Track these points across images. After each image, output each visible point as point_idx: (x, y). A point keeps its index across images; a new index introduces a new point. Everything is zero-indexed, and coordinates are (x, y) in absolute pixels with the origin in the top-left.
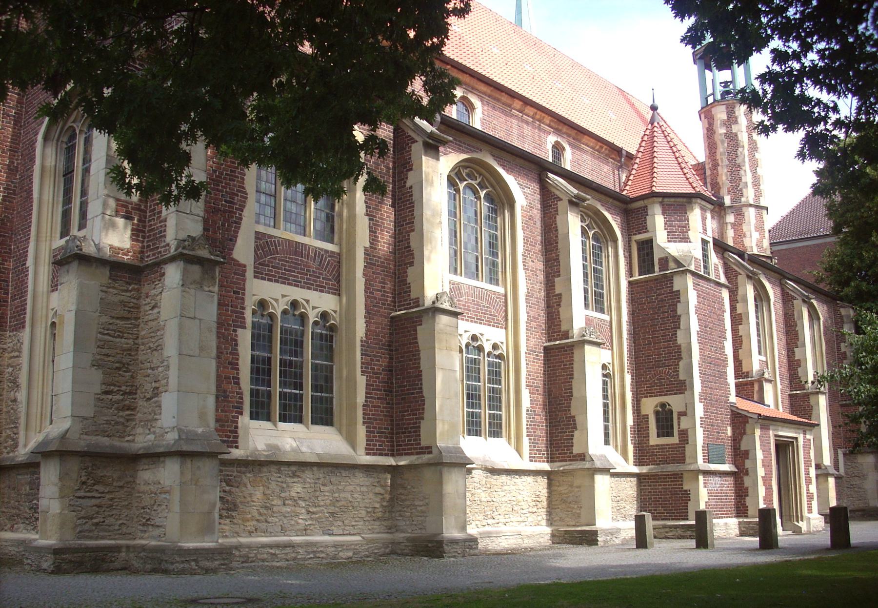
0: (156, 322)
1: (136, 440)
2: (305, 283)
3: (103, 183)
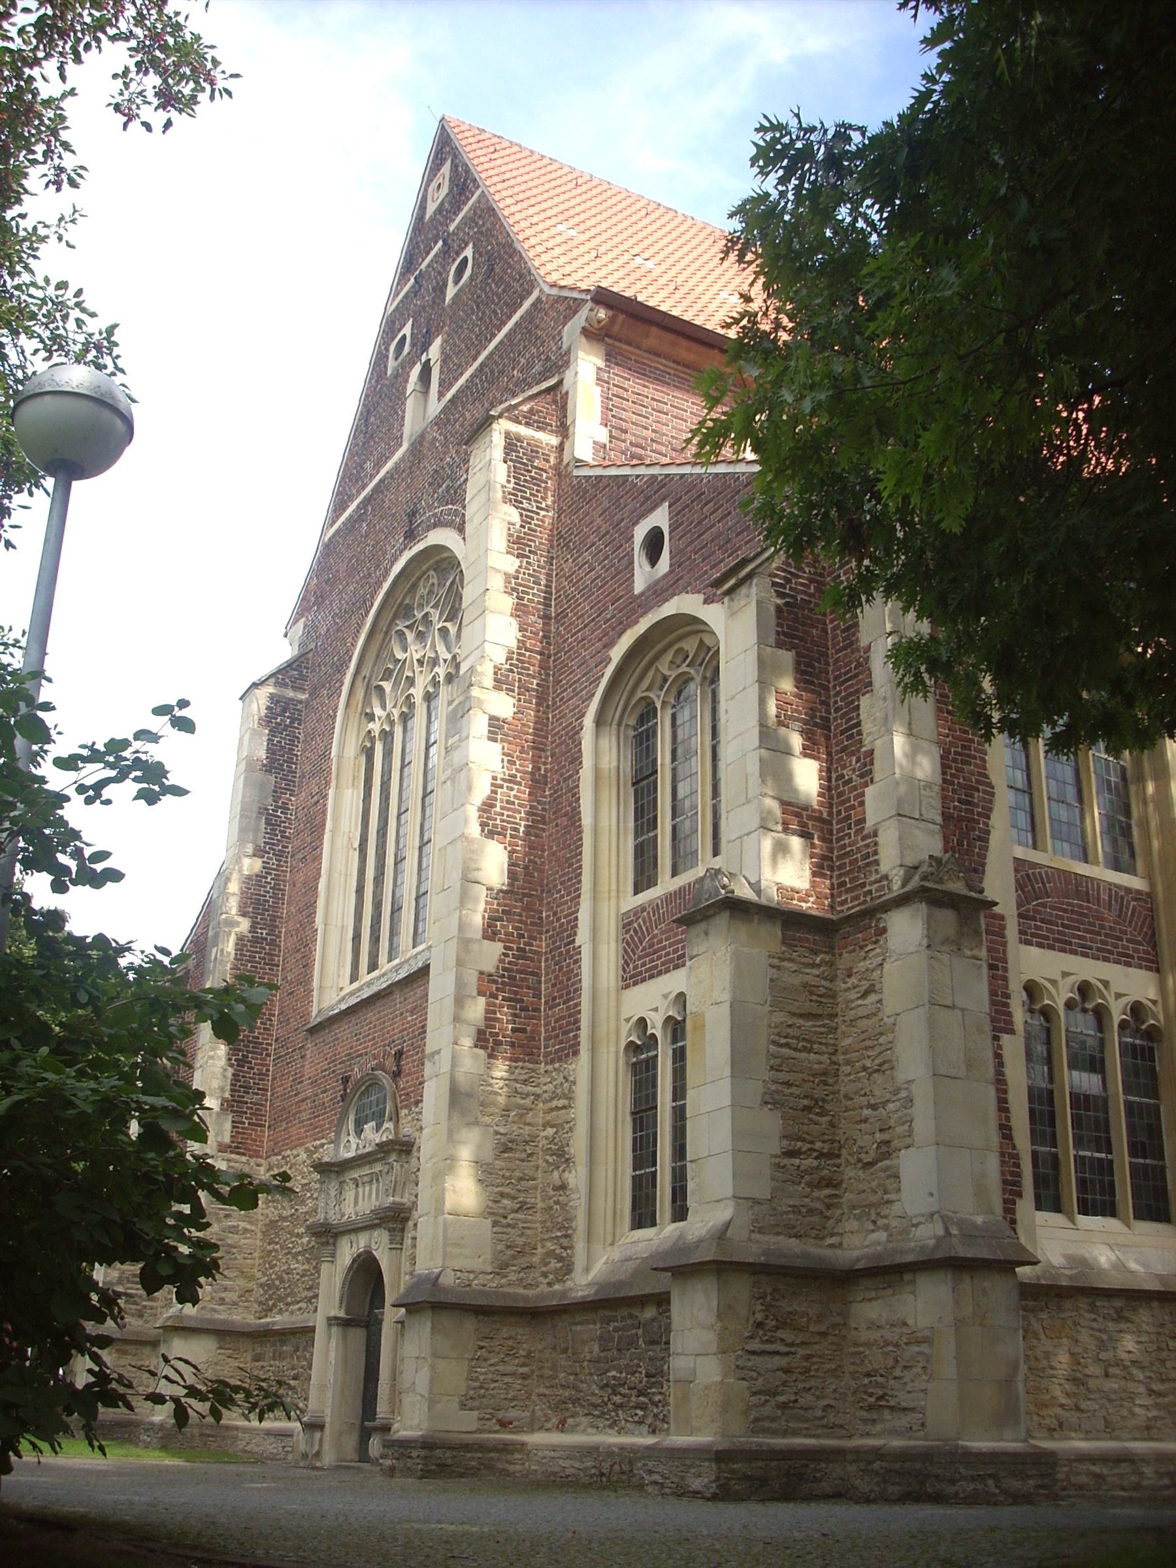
0: (875, 1020)
1: (845, 1245)
2: (1099, 949)
3: (757, 774)
